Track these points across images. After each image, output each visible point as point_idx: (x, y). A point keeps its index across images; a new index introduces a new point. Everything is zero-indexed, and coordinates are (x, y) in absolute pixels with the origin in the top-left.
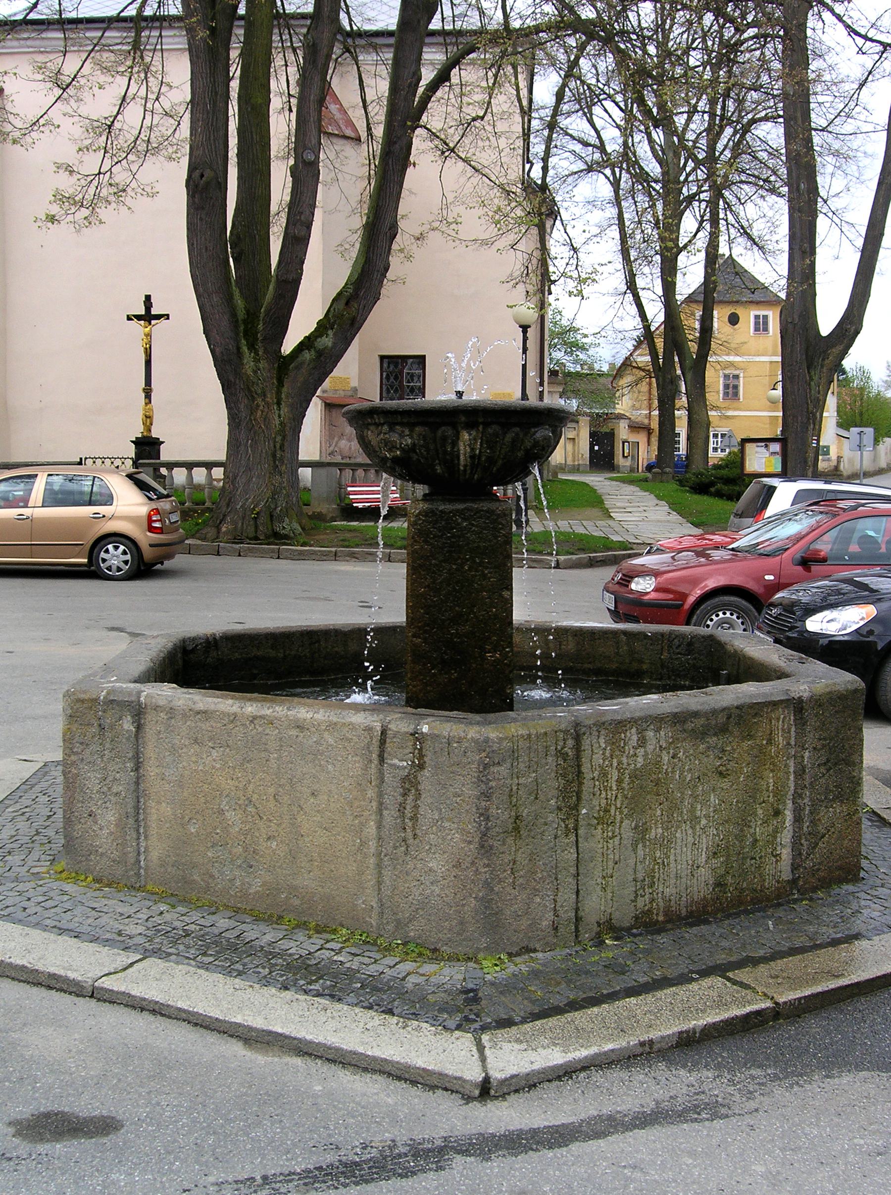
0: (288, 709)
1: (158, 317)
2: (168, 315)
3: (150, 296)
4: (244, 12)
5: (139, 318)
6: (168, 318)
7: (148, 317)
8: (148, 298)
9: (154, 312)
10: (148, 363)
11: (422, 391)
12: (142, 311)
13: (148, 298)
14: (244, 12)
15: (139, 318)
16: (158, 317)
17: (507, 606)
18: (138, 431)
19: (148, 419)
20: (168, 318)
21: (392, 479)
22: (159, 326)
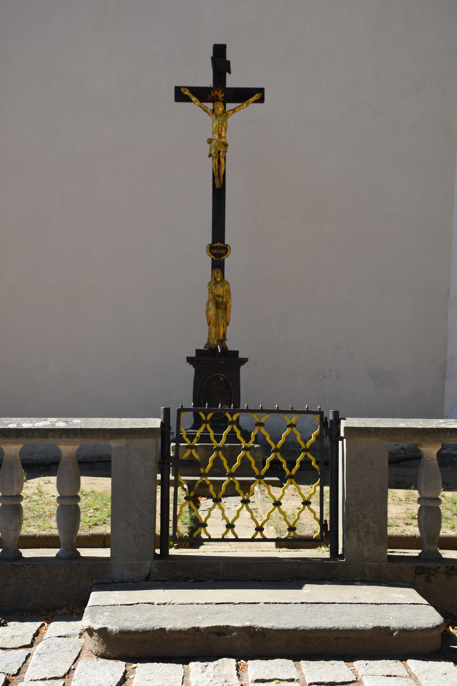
0: (424, 566)
1: (243, 95)
2: (261, 91)
3: (223, 47)
4: (158, 475)
5: (202, 94)
6: (261, 100)
7: (221, 91)
8: (219, 52)
9: (232, 81)
10: (219, 194)
11: (239, 408)
12: (206, 80)
13: (219, 52)
14: (158, 475)
15: (202, 94)
16: (243, 95)
17: (83, 476)
18: (199, 340)
19: (220, 305)
20: (261, 100)
21: (24, 522)
22: (242, 116)
